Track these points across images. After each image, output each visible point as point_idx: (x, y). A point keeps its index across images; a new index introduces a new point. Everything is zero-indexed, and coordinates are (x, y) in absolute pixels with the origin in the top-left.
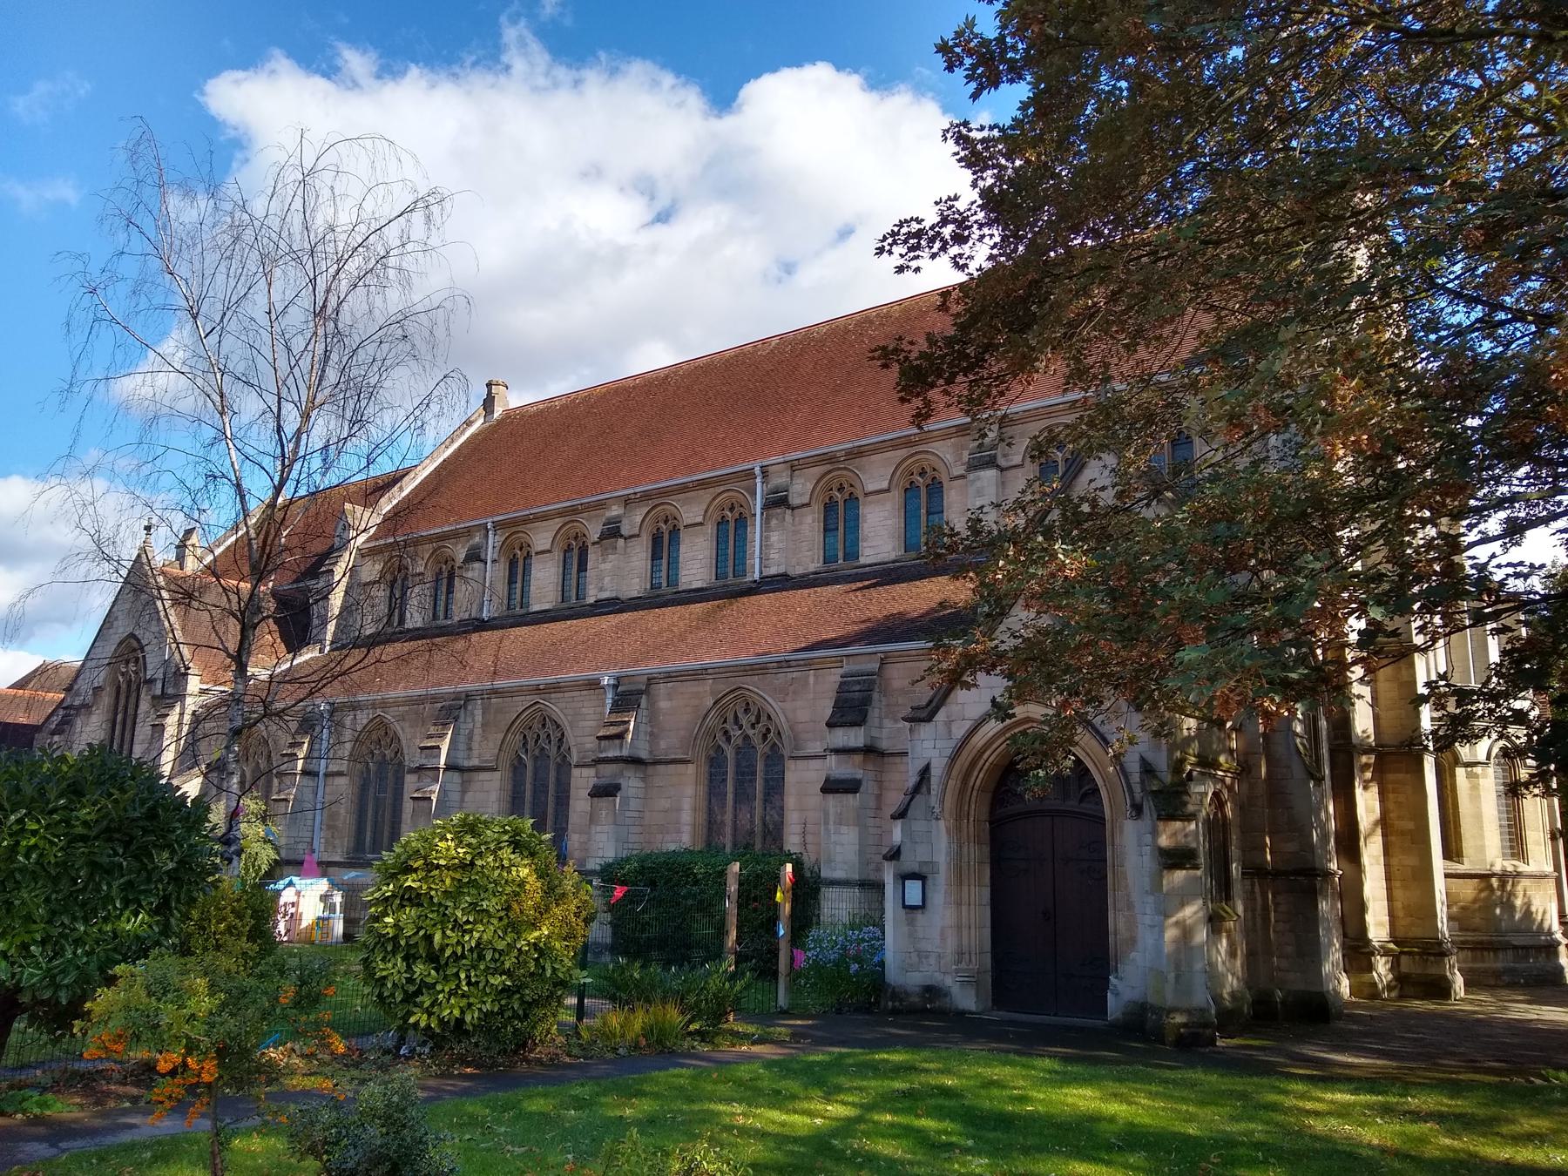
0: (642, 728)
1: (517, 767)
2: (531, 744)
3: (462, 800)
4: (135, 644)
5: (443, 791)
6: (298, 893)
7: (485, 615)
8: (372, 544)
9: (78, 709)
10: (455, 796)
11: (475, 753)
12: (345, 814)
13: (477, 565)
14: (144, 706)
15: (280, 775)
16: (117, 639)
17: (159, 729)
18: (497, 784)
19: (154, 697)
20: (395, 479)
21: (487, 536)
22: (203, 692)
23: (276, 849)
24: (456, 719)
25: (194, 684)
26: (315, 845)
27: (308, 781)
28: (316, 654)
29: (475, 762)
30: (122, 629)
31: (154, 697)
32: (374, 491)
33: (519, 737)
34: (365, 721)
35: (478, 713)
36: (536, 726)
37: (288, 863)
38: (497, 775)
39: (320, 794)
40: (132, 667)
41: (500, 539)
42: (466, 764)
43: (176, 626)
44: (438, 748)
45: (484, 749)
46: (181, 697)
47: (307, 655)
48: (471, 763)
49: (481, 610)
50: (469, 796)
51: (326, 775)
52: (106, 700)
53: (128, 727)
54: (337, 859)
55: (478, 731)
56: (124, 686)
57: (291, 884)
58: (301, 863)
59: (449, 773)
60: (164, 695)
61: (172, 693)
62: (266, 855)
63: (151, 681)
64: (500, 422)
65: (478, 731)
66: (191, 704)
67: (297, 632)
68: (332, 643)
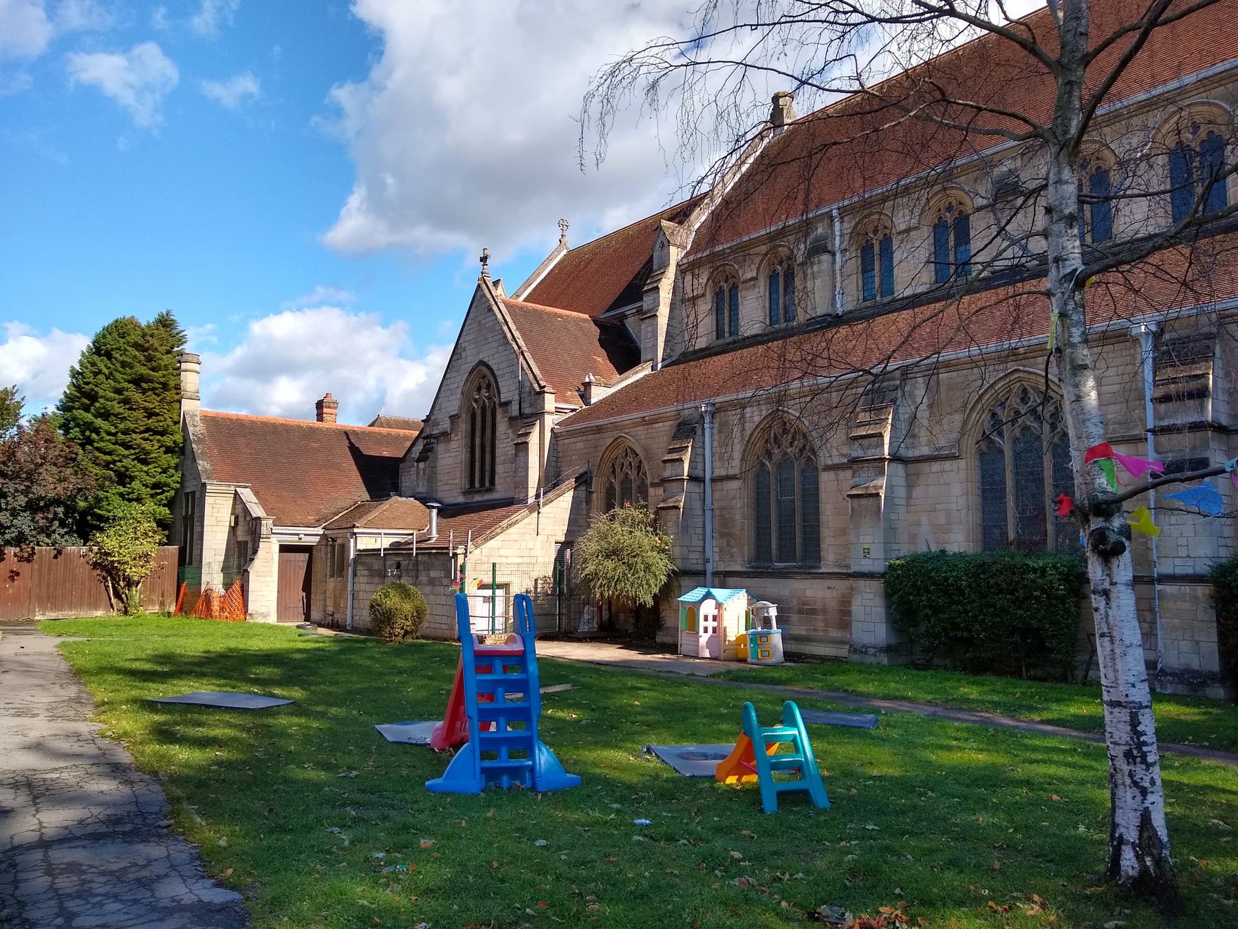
0: (1220, 382)
1: (988, 457)
2: (618, 470)
3: (909, 497)
4: (485, 370)
5: (890, 488)
6: (719, 606)
7: (840, 311)
8: (691, 258)
9: (437, 437)
10: (901, 492)
11: (923, 436)
12: (742, 521)
13: (825, 257)
14: (502, 426)
15: (664, 481)
16: (467, 368)
17: (522, 447)
18: (962, 474)
19: (512, 419)
20: (694, 203)
21: (831, 225)
22: (558, 411)
23: (672, 559)
24: (894, 401)
25: (550, 402)
26: (709, 554)
27: (696, 488)
28: (648, 371)
29: (925, 451)
30: (470, 360)
31: (512, 419)
32: (680, 214)
33: (986, 416)
34: (757, 419)
35: (920, 392)
36: (1014, 401)
37: (686, 573)
38: (962, 463)
39: (708, 500)
40: (484, 393)
41: (848, 226)
42: (911, 453)
43: (524, 348)
44: (680, 460)
45: (946, 432)
46: (540, 414)
47: (641, 373)
48: (917, 453)
49: (833, 303)
50: (918, 492)
51: (713, 480)
52: (463, 427)
53: (488, 450)
54: (737, 568)
55: (923, 413)
56: (479, 412)
57: (708, 596)
58: (703, 573)
59: (893, 465)
60: (522, 415)
61: (530, 415)
62: (662, 566)
63: (507, 404)
64: (791, 134)
65: (923, 413)
66: (550, 421)
67: (624, 352)
68: (663, 360)
